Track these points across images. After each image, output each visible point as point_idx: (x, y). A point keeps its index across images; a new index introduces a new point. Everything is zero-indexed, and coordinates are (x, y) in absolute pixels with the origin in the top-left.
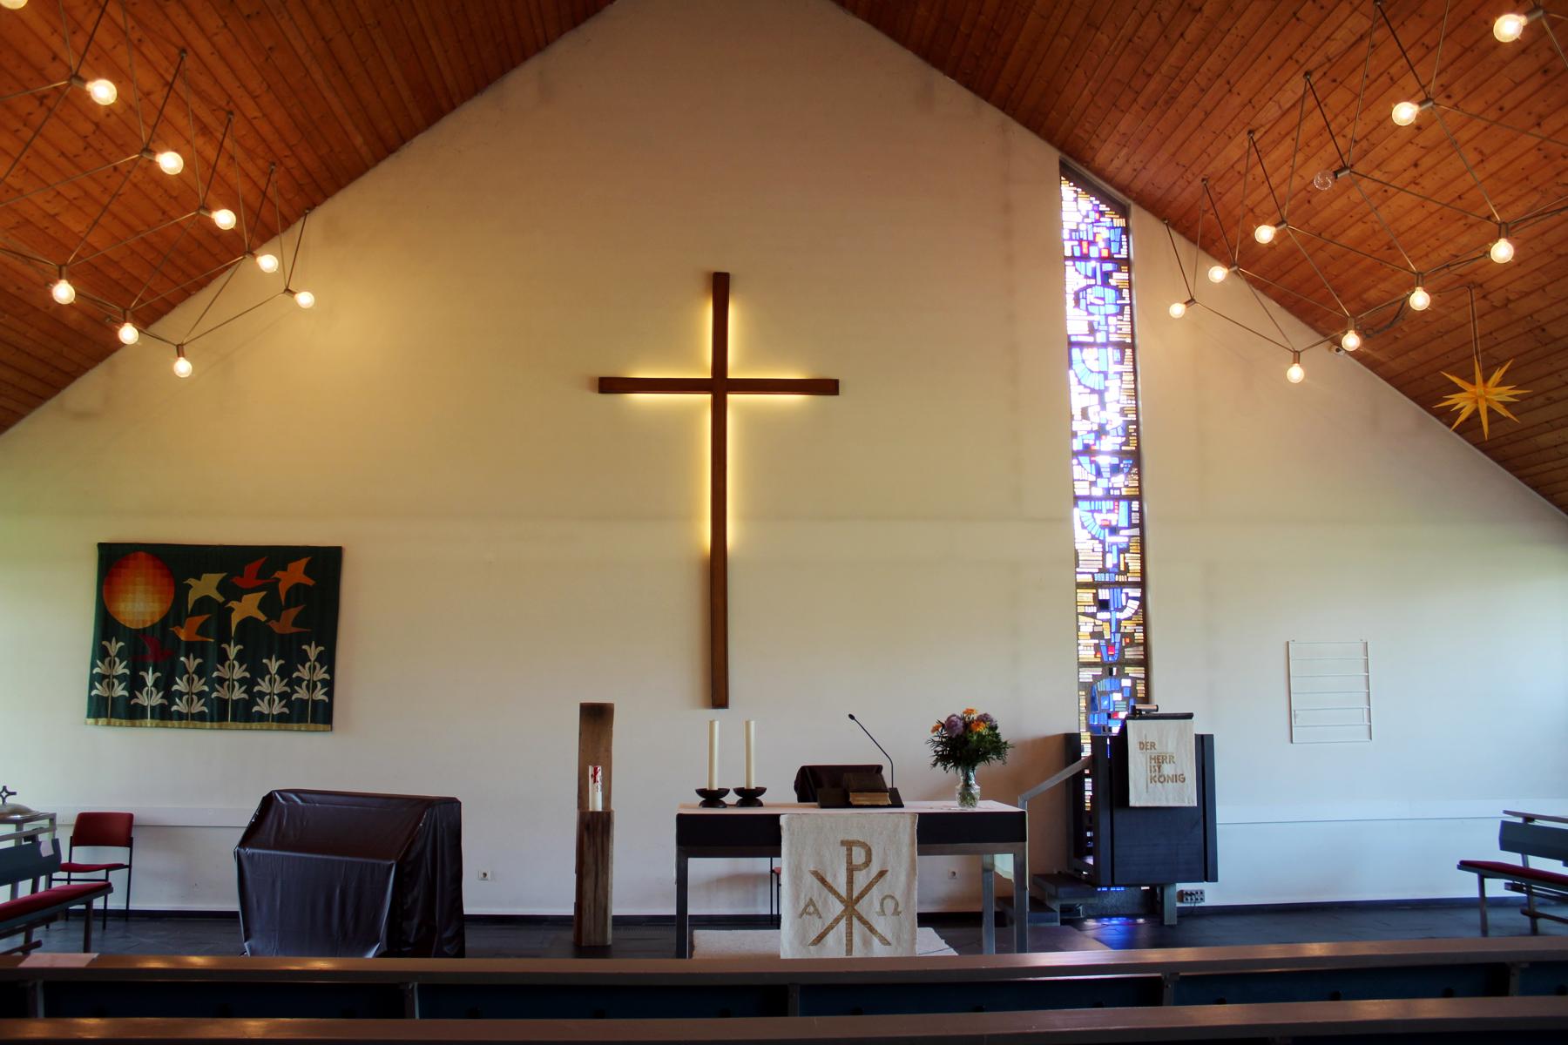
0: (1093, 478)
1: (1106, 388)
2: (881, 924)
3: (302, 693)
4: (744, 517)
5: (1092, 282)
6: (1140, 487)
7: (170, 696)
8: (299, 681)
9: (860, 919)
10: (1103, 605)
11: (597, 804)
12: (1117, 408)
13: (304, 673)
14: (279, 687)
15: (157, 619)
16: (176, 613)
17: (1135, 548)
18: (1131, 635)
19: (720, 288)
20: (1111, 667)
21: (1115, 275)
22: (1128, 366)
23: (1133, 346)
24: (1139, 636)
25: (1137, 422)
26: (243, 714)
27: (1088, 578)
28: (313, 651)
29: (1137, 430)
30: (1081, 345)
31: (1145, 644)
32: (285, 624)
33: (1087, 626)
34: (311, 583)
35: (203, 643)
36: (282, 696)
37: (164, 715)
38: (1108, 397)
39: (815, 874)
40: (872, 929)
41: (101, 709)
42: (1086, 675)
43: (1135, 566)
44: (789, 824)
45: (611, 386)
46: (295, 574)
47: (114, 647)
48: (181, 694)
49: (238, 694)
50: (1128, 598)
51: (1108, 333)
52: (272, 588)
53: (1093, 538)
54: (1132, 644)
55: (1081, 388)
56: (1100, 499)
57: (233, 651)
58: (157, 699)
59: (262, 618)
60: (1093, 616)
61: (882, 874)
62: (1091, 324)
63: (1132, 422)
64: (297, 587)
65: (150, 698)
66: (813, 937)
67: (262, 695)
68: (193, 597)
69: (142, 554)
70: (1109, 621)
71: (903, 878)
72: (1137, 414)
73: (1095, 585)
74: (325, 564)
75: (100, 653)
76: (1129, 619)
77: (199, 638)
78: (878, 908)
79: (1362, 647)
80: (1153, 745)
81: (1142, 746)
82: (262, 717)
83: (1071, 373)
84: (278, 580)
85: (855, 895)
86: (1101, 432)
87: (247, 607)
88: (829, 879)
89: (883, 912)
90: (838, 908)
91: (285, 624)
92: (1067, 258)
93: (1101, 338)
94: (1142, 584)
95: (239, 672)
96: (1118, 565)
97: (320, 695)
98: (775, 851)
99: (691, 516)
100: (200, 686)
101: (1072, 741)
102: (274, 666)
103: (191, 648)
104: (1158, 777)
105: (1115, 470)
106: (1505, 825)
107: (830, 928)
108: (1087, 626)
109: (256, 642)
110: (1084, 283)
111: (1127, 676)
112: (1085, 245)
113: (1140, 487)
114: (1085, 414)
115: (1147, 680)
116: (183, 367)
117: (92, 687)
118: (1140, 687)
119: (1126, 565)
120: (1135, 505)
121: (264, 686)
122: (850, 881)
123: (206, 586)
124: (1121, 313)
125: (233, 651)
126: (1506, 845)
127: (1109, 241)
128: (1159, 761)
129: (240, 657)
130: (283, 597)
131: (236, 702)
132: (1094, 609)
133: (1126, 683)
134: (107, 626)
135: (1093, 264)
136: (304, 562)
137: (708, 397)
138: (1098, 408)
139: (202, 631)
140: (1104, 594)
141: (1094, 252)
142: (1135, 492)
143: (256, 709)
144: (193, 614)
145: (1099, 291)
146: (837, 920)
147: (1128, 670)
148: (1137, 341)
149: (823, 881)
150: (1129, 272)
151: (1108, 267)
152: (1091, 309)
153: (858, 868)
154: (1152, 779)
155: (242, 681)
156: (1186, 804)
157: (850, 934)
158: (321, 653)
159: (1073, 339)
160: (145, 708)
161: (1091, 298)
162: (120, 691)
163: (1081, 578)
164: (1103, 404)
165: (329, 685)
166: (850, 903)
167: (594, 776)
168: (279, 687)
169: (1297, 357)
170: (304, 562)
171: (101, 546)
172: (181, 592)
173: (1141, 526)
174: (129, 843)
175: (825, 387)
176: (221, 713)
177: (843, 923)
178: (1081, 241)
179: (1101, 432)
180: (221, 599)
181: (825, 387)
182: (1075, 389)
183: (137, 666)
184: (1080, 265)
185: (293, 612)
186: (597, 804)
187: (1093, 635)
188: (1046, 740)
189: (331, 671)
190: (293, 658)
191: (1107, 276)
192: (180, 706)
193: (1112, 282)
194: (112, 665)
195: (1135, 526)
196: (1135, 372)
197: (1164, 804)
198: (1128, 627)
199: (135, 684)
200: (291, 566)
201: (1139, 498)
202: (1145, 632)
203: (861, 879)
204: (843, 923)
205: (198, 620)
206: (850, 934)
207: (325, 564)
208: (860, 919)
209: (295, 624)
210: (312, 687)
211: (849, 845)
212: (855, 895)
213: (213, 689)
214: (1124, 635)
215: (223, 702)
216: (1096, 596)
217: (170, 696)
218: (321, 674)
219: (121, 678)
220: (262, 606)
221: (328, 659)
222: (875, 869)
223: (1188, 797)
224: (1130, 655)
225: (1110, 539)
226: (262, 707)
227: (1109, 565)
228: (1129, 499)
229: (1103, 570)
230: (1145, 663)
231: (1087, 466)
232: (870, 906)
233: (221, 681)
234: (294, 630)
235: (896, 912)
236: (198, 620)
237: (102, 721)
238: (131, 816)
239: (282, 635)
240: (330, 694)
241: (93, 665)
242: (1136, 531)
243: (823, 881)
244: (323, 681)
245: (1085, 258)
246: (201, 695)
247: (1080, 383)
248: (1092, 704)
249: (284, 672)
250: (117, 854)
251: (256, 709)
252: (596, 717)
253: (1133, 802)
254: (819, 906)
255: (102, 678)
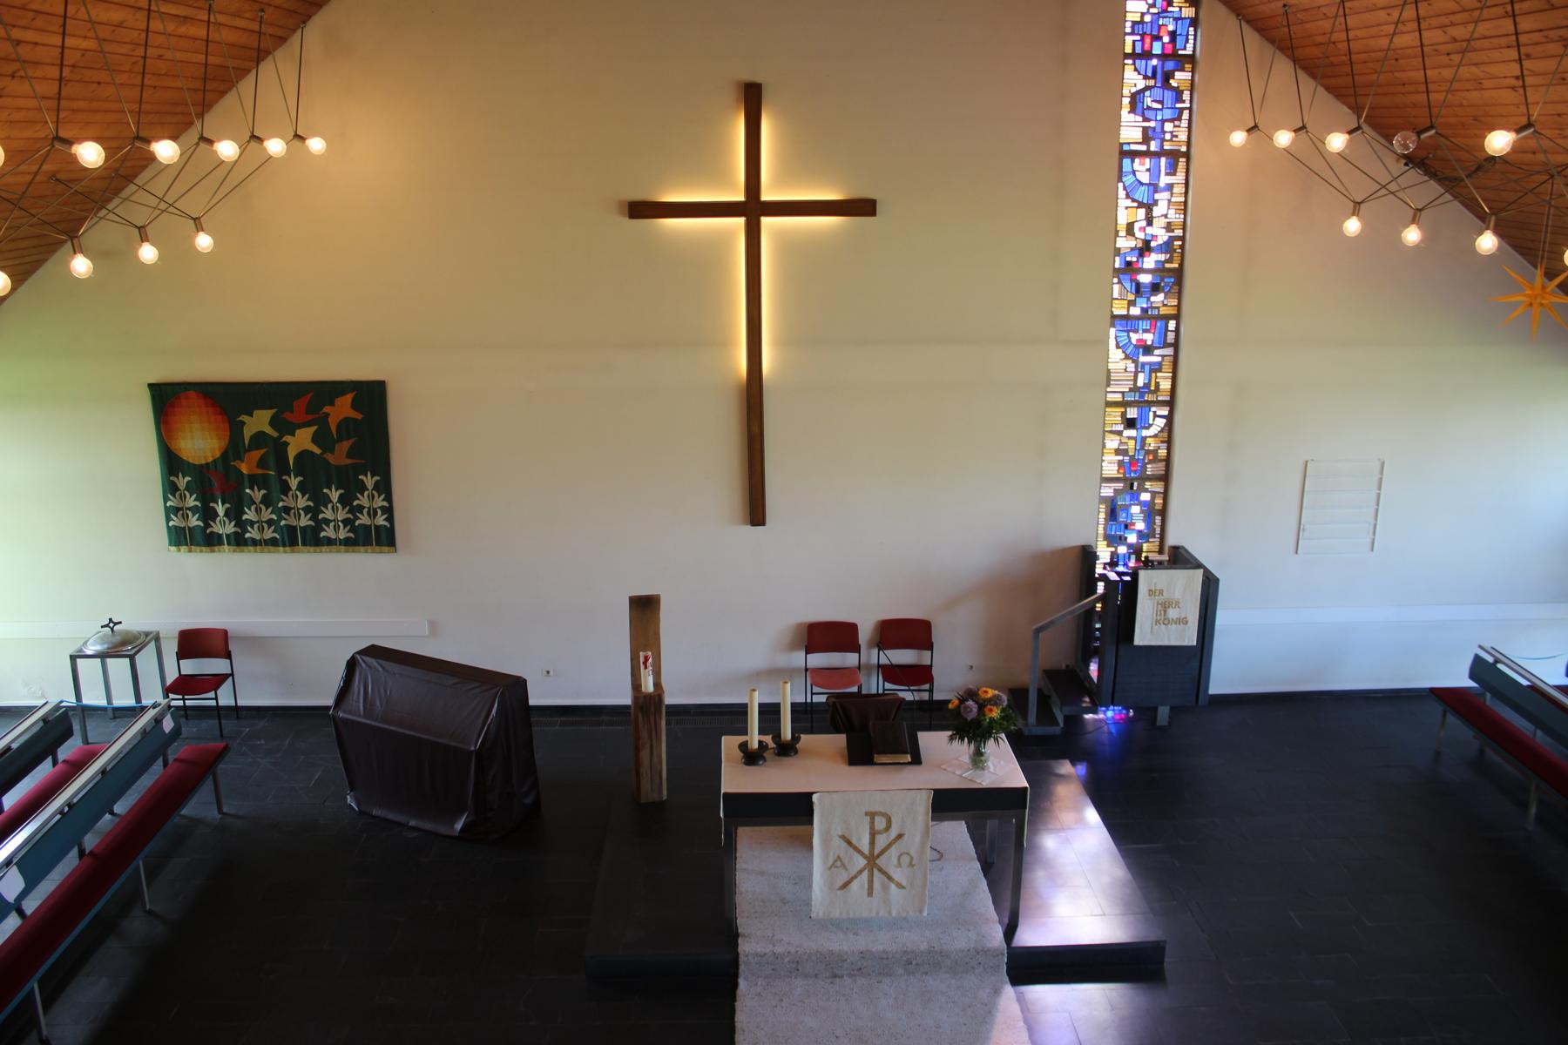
0: (1131, 297)
1: (1156, 202)
2: (897, 875)
3: (364, 519)
4: (778, 343)
5: (1151, 83)
6: (1179, 306)
7: (242, 525)
8: (360, 508)
9: (880, 870)
10: (1130, 424)
11: (648, 686)
12: (1163, 222)
13: (363, 500)
14: (342, 514)
15: (218, 454)
16: (234, 449)
17: (1167, 366)
18: (1155, 452)
19: (752, 99)
20: (1131, 481)
21: (1178, 75)
22: (1180, 177)
23: (1187, 155)
24: (1163, 452)
25: (1182, 239)
26: (313, 538)
27: (1118, 397)
28: (369, 481)
29: (1182, 247)
30: (1133, 155)
31: (1168, 460)
32: (340, 456)
33: (1112, 443)
34: (359, 416)
35: (264, 475)
36: (346, 522)
37: (239, 541)
38: (1157, 211)
39: (843, 837)
40: (890, 878)
41: (180, 537)
42: (1108, 491)
43: (1166, 385)
44: (820, 800)
45: (644, 210)
46: (342, 409)
47: (182, 481)
48: (252, 523)
49: (305, 521)
50: (1155, 416)
51: (1163, 140)
52: (323, 422)
53: (1127, 357)
54: (1156, 460)
55: (1129, 203)
56: (1138, 318)
57: (294, 482)
58: (230, 528)
59: (317, 451)
60: (1119, 433)
61: (900, 836)
62: (1145, 130)
63: (1178, 238)
64: (347, 420)
65: (224, 528)
66: (840, 884)
67: (327, 522)
68: (248, 433)
69: (192, 393)
70: (1135, 439)
71: (918, 839)
72: (1184, 229)
73: (1124, 404)
74: (371, 398)
75: (171, 488)
76: (1155, 436)
77: (260, 471)
78: (895, 861)
79: (1378, 464)
80: (1161, 592)
81: (1151, 593)
82: (330, 542)
83: (1120, 185)
84: (327, 415)
85: (876, 852)
86: (1145, 248)
87: (301, 441)
88: (854, 841)
89: (899, 865)
90: (862, 862)
91: (340, 456)
92: (1127, 56)
93: (1154, 146)
94: (1171, 404)
95: (302, 502)
96: (1147, 386)
97: (381, 520)
99: (726, 343)
100: (267, 514)
101: (1087, 555)
102: (335, 495)
103: (254, 481)
104: (1162, 619)
105: (1155, 288)
106: (1477, 659)
107: (855, 877)
108: (1112, 443)
109: (314, 474)
110: (1141, 84)
111: (1146, 490)
112: (1148, 40)
113: (1179, 306)
114: (1130, 229)
115: (1166, 495)
116: (204, 241)
117: (168, 519)
118: (1159, 501)
119: (1157, 384)
120: (1172, 325)
121: (327, 514)
122: (872, 843)
123: (259, 422)
124: (1179, 118)
125: (294, 482)
127: (1173, 35)
128: (1166, 606)
129: (302, 488)
130: (333, 428)
131: (304, 529)
132: (1120, 428)
134: (172, 463)
135: (1154, 62)
136: (349, 398)
137: (741, 221)
138: (1144, 223)
139: (262, 463)
140: (1132, 413)
141: (1157, 49)
142: (1173, 311)
143: (323, 534)
144: (250, 449)
145: (1158, 92)
146: (861, 872)
147: (1148, 485)
148: (1193, 151)
149: (849, 843)
150: (1193, 71)
151: (1170, 65)
152: (1149, 114)
153: (880, 832)
154: (1157, 622)
155: (307, 510)
156: (1186, 643)
157: (871, 882)
158: (377, 483)
159: (1126, 148)
160: (220, 536)
161: (1148, 101)
162: (194, 521)
163: (1111, 397)
164: (1150, 222)
165: (389, 511)
166: (872, 860)
167: (645, 663)
168: (342, 514)
169: (1356, 208)
170: (349, 398)
171: (152, 387)
172: (236, 429)
173: (1176, 345)
174: (228, 656)
175: (860, 207)
176: (290, 539)
177: (865, 873)
178: (1143, 36)
179: (1145, 248)
180: (275, 434)
181: (860, 207)
182: (1123, 202)
183: (206, 499)
184: (1141, 64)
185: (346, 445)
186: (648, 686)
187: (1118, 452)
188: (1065, 551)
189: (389, 498)
190: (351, 490)
191: (1168, 76)
192: (252, 533)
193: (1173, 83)
194: (183, 498)
195: (1170, 345)
197: (1166, 643)
198: (1152, 444)
199: (208, 515)
200: (338, 401)
201: (1177, 317)
202: (1169, 449)
203: (881, 841)
204: (865, 873)
205: (256, 455)
206: (871, 882)
207: (371, 398)
208: (880, 870)
209: (349, 456)
210: (373, 513)
211: (872, 815)
212: (876, 852)
213: (281, 518)
214: (1148, 452)
215: (291, 530)
216: (1124, 415)
217: (242, 525)
218: (380, 502)
219: (194, 510)
220: (316, 439)
221: (385, 487)
222: (894, 833)
223: (1190, 638)
224: (1151, 473)
225: (1143, 359)
226: (329, 532)
227: (1140, 383)
228: (1167, 318)
229: (1134, 389)
230: (1165, 478)
231: (1128, 285)
232: (889, 861)
233: (287, 510)
234: (348, 462)
235: (911, 865)
236: (256, 455)
237: (183, 548)
238: (225, 632)
239: (338, 467)
240: (390, 519)
241: (166, 500)
242: (1170, 351)
243: (849, 843)
244: (382, 508)
245: (1147, 55)
246: (270, 522)
247: (1128, 196)
248: (1112, 514)
249: (345, 500)
250: (215, 666)
251: (323, 534)
252: (644, 608)
253: (1138, 641)
254: (846, 861)
255: (177, 510)
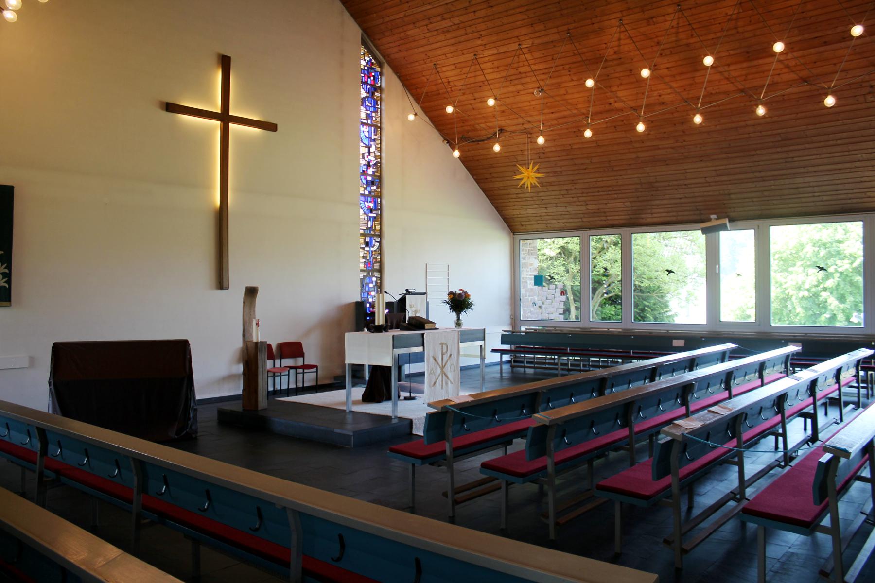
10: (367, 244)
18: (376, 258)
24: (379, 258)
45: (172, 108)
54: (376, 262)
60: (363, 249)
94: (380, 236)
98: (363, 366)
120: (522, 38)
126: (503, 343)
133: (374, 279)
140: (367, 239)
181: (269, 127)
187: (364, 257)
188: (349, 304)
196: (381, 139)
211: (442, 344)
225: (370, 215)
229: (367, 228)
230: (380, 270)
